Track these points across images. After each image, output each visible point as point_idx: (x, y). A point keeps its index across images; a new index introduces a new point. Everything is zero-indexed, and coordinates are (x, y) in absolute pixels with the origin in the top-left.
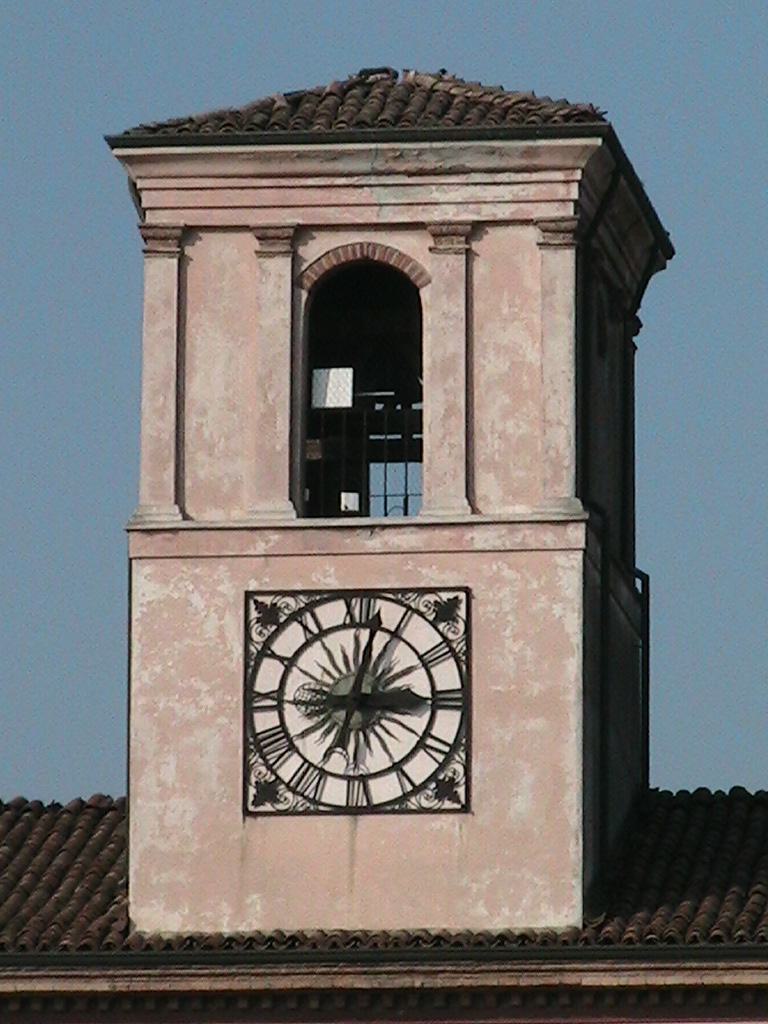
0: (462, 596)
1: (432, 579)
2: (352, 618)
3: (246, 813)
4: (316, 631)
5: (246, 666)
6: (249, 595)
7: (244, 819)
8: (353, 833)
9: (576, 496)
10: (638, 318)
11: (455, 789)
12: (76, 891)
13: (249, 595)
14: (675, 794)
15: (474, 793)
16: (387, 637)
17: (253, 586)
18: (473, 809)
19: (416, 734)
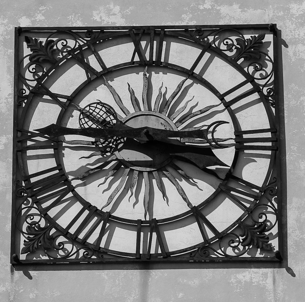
0: (269, 38)
1: (231, 17)
2: (141, 56)
3: (16, 264)
4: (99, 69)
5: (17, 105)
6: (19, 31)
7: (12, 271)
8: (144, 285)
9: (280, 31)
10: (264, 42)
11: (270, 242)
12: (25, 203)
13: (19, 31)
14: (268, 49)
15: (290, 242)
16: (83, 123)
17: (25, 23)
18: (291, 262)
19: (232, 139)
